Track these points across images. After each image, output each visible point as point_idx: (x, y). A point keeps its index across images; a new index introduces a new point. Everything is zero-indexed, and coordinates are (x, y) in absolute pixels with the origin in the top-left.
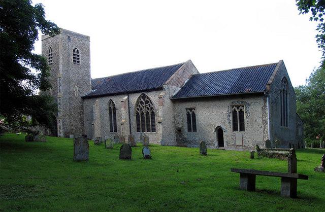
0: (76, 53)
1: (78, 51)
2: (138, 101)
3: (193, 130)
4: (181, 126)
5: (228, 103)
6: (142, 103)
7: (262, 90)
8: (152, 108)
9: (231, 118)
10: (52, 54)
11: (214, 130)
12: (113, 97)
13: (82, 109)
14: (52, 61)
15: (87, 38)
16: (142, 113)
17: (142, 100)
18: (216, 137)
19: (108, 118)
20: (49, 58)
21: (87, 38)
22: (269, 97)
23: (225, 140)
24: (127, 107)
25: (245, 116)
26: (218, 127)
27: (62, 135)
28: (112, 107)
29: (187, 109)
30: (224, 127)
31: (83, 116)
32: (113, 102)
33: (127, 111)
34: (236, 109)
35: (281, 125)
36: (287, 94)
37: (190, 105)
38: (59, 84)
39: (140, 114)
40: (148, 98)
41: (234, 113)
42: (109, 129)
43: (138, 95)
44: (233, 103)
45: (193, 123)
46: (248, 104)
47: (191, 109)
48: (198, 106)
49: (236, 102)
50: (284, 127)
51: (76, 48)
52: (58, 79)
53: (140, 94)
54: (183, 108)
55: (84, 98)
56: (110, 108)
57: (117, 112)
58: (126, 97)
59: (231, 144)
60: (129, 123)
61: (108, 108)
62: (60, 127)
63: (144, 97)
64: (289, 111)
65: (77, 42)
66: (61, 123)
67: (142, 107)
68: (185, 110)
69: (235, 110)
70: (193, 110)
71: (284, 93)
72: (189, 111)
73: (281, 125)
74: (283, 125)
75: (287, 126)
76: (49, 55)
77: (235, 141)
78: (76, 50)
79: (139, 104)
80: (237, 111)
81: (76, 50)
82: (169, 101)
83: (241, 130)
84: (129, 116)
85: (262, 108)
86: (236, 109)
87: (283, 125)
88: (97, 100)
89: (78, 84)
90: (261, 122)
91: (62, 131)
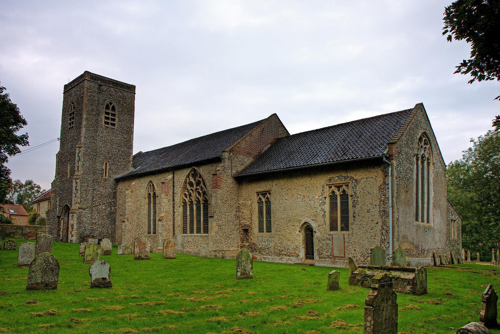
0: (110, 111)
1: (113, 109)
2: (185, 182)
3: (267, 229)
4: (248, 223)
5: (321, 181)
6: (191, 184)
7: (377, 153)
8: (204, 193)
9: (327, 207)
10: (73, 113)
11: (298, 229)
12: (154, 177)
13: (115, 197)
14: (73, 122)
15: (131, 89)
16: (191, 202)
17: (192, 180)
18: (301, 242)
19: (146, 212)
20: (70, 119)
21: (131, 89)
22: (392, 165)
23: (315, 248)
24: (171, 193)
25: (350, 203)
26: (306, 223)
27: (74, 239)
28: (152, 193)
29: (258, 194)
30: (314, 225)
31: (115, 209)
32: (153, 185)
33: (171, 198)
34: (336, 191)
35: (417, 220)
36: (428, 164)
37: (263, 186)
38: (77, 158)
39: (202, 202)
40: (200, 177)
41: (333, 197)
42: (146, 229)
43: (187, 172)
44: (330, 180)
45: (267, 218)
46: (356, 181)
47: (264, 194)
48: (275, 187)
49: (336, 178)
50: (421, 224)
51: (111, 104)
52: (77, 151)
53: (189, 170)
54: (251, 192)
55: (118, 181)
56: (149, 194)
57: (157, 202)
58: (170, 177)
59: (325, 254)
60: (349, 157)
61: (147, 196)
62: (72, 225)
63: (195, 174)
64: (432, 194)
65: (114, 93)
66: (75, 219)
67: (191, 191)
68: (256, 195)
69: (333, 192)
70: (268, 195)
71: (423, 162)
72: (260, 196)
73: (417, 220)
74: (420, 219)
75: (428, 221)
76: (71, 115)
77: (332, 250)
78: (111, 107)
79: (188, 186)
80: (338, 193)
81: (111, 107)
82: (231, 181)
83: (342, 229)
84: (174, 207)
85: (380, 188)
86: (336, 191)
87: (420, 219)
88: (133, 183)
89: (110, 158)
90: (377, 215)
91: (74, 232)
